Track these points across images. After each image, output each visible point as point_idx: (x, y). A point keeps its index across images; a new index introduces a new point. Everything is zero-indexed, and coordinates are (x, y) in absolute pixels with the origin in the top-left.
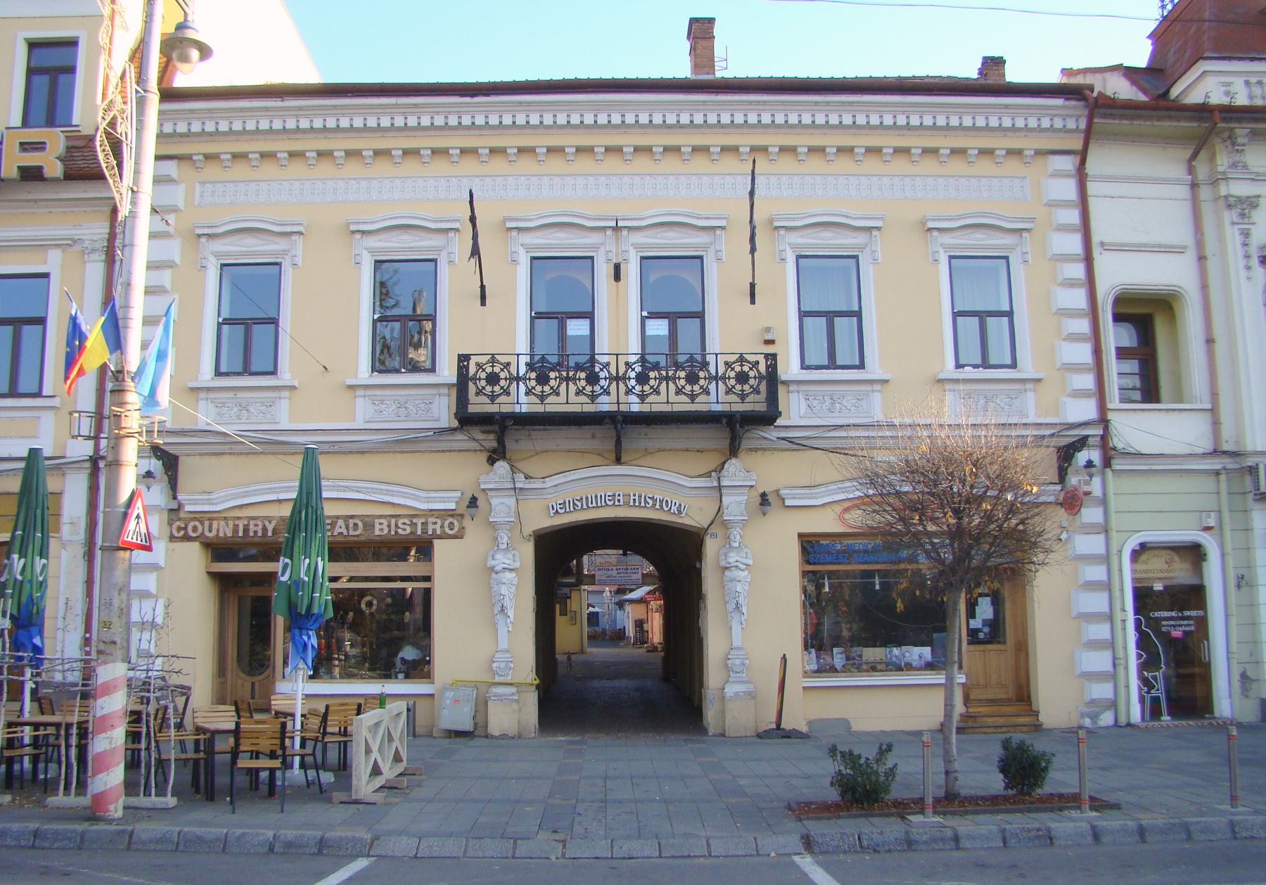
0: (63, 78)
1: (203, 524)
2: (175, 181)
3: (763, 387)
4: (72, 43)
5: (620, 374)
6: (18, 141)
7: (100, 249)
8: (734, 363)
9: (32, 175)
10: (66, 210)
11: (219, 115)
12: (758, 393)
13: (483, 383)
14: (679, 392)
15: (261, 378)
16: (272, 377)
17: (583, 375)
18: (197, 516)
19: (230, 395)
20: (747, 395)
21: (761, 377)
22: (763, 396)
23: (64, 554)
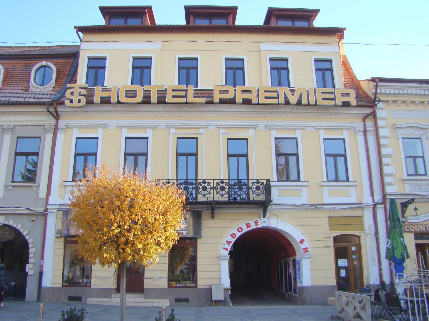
0: (100, 71)
1: (414, 226)
2: (383, 109)
4: (104, 59)
5: (215, 186)
6: (340, 93)
9: (346, 105)
11: (400, 88)
14: (217, 193)
15: (422, 176)
16: (426, 176)
17: (237, 187)
18: (412, 224)
19: (415, 182)
20: (260, 194)
23: (367, 238)
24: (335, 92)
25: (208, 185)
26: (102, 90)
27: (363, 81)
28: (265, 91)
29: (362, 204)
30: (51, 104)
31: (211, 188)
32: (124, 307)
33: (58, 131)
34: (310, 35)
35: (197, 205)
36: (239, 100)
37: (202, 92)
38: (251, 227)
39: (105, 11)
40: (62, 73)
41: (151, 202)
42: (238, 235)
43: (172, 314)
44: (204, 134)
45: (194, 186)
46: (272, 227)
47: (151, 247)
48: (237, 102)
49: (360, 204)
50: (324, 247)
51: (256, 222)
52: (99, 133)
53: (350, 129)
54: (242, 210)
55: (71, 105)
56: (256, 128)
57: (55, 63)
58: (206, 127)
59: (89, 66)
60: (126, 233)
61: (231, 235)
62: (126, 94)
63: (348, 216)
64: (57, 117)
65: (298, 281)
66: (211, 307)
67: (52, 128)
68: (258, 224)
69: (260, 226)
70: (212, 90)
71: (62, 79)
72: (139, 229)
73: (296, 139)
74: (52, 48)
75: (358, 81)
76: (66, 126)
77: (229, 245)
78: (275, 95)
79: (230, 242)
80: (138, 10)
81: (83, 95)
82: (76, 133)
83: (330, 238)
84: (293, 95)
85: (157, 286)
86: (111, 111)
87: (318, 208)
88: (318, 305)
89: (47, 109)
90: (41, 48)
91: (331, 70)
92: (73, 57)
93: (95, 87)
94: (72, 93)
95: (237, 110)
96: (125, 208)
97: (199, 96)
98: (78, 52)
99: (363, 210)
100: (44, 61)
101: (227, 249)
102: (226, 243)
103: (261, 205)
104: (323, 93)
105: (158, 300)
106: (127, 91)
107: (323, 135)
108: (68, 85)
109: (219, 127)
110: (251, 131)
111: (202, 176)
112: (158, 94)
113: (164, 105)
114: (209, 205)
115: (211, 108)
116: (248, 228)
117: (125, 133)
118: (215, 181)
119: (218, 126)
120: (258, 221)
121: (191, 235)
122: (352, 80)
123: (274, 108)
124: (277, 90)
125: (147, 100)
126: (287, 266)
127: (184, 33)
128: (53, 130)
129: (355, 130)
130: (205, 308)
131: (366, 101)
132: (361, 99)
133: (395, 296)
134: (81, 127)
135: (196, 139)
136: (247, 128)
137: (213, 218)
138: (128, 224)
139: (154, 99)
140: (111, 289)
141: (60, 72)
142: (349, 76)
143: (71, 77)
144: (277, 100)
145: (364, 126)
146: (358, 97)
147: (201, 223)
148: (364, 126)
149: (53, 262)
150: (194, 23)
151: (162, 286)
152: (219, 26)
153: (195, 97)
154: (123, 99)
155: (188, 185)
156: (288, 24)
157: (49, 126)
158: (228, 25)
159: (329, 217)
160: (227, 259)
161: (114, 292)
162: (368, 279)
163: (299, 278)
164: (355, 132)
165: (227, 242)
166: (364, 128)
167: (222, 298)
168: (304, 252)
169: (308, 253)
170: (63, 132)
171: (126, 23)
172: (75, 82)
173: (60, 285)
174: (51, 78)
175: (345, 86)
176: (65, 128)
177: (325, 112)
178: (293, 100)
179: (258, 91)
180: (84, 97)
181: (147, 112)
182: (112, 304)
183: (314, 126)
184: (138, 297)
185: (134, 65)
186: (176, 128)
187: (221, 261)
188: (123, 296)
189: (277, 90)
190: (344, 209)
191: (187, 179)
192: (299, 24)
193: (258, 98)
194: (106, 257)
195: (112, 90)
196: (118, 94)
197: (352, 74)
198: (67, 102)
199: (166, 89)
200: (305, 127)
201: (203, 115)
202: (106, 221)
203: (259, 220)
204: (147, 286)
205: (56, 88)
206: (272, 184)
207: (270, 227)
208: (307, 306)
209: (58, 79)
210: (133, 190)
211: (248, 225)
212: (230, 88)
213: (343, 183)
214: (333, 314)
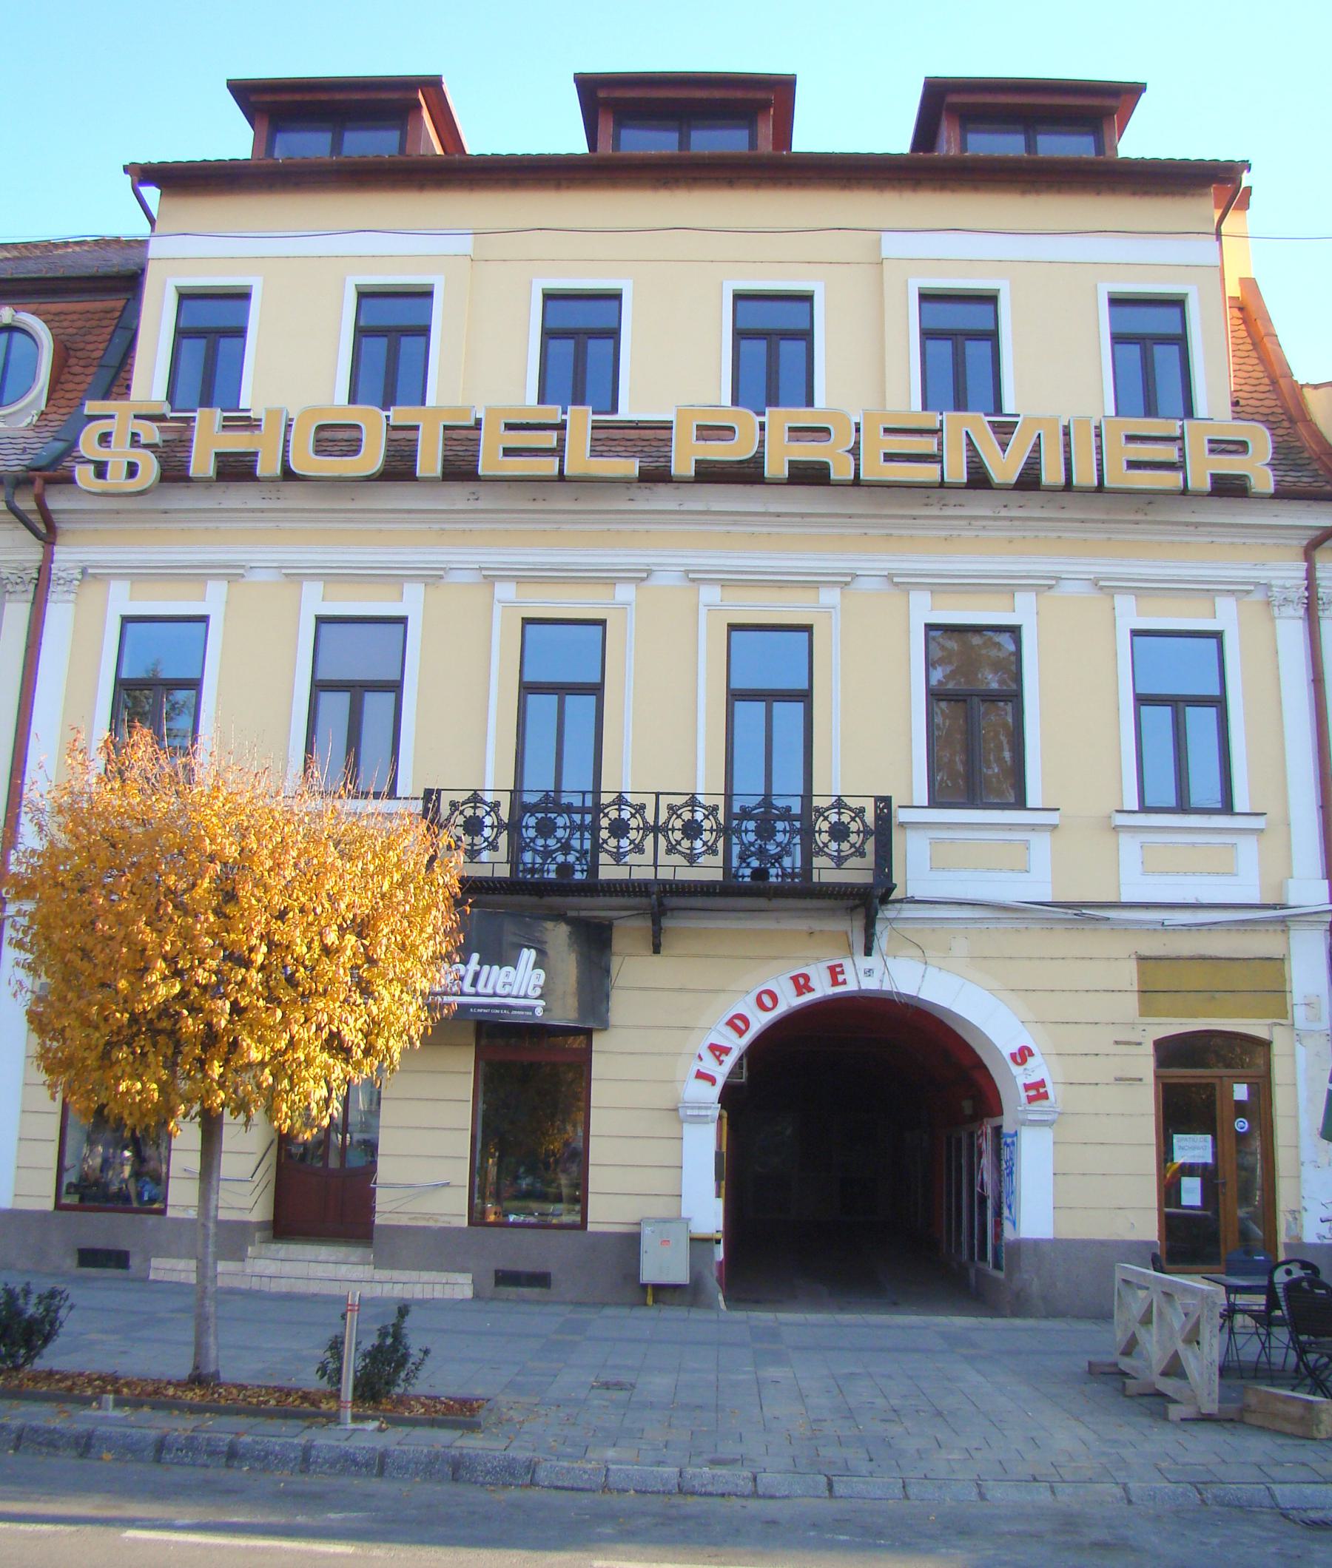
3: (870, 846)
4: (243, 296)
5: (661, 821)
7: (1296, 601)
8: (828, 809)
10: (1236, 540)
12: (862, 855)
13: (678, 835)
14: (671, 849)
17: (751, 825)
21: (866, 832)
22: (870, 859)
23: (1300, 1050)
24: (1183, 433)
25: (853, 819)
26: (224, 426)
27: (1316, 387)
28: (887, 431)
29: (1283, 907)
30: (22, 482)
31: (574, 828)
32: (211, 1289)
33: (52, 589)
34: (1098, 194)
35: (592, 896)
36: (776, 467)
37: (633, 431)
38: (811, 990)
39: (253, 98)
40: (79, 354)
41: (311, 881)
42: (760, 1021)
43: (397, 1326)
44: (634, 604)
45: (797, 824)
46: (898, 994)
47: (309, 1062)
48: (766, 474)
49: (1274, 907)
50: (1112, 1080)
51: (835, 972)
52: (212, 600)
53: (1248, 592)
54: (777, 920)
55: (98, 485)
56: (847, 584)
57: (55, 314)
58: (642, 579)
59: (550, 325)
60: (206, 1001)
61: (730, 1023)
62: (317, 441)
63: (1223, 956)
64: (47, 532)
65: (1007, 1218)
66: (640, 1312)
67: (27, 578)
68: (840, 978)
69: (851, 987)
70: (667, 426)
71: (77, 379)
72: (257, 987)
73: (1217, 636)
74: (60, 252)
75: (1297, 389)
76: (84, 572)
77: (721, 1062)
78: (926, 445)
79: (726, 1051)
80: (384, 96)
81: (147, 446)
82: (122, 599)
83: (1139, 1044)
84: (1004, 446)
85: (424, 1219)
86: (262, 511)
87: (1098, 919)
88: (1078, 1317)
89: (8, 503)
90: (16, 253)
91: (1181, 341)
92: (126, 290)
93: (195, 411)
94: (105, 438)
95: (773, 509)
96: (199, 901)
97: (618, 449)
98: (143, 270)
99: (1286, 931)
100: (7, 308)
101: (712, 1080)
102: (708, 1057)
103: (857, 902)
104: (1130, 438)
105: (426, 1276)
106: (321, 428)
107: (1130, 614)
108: (88, 404)
109: (695, 578)
110: (830, 596)
111: (828, 784)
112: (593, 439)
113: (472, 486)
114: (641, 896)
115: (662, 499)
116: (800, 993)
117: (316, 600)
118: (664, 801)
119: (691, 576)
120: (841, 965)
121: (566, 1014)
122: (1274, 382)
123: (926, 501)
124: (938, 426)
125: (401, 466)
126: (974, 1153)
127: (568, 188)
128: (32, 587)
129: (1270, 601)
130: (609, 1311)
131: (1321, 472)
132: (1297, 467)
133: (1323, 1292)
134: (140, 576)
135: (601, 627)
136: (812, 583)
137: (657, 949)
138: (212, 963)
139: (429, 461)
140: (243, 1226)
141: (71, 352)
142: (1260, 368)
143: (113, 371)
144: (938, 466)
145: (1306, 579)
146: (1285, 456)
147: (608, 971)
148: (1306, 579)
149: (24, 1111)
150: (616, 146)
151: (446, 1218)
152: (711, 157)
153: (595, 453)
154: (306, 461)
155: (553, 816)
156: (1008, 145)
157: (16, 568)
158: (685, 153)
159: (1142, 959)
160: (709, 1119)
161: (257, 1235)
162: (1295, 1219)
163: (1010, 1207)
164: (1269, 603)
165: (713, 1048)
166: (1307, 589)
167: (680, 1275)
168: (1031, 1099)
169: (1044, 1102)
170: (72, 597)
171: (684, 143)
172: (125, 391)
173: (49, 1205)
174: (34, 377)
175: (1238, 409)
176: (80, 577)
177: (1139, 517)
178: (1004, 467)
179: (858, 430)
180: (153, 456)
181: (406, 516)
182: (243, 1284)
183: (1092, 577)
184: (353, 1259)
185: (362, 323)
186: (519, 580)
187: (686, 1126)
188: (207, 1247)
189: (938, 426)
190: (1206, 927)
191: (768, 795)
192: (1056, 146)
193: (857, 459)
194: (128, 1090)
195: (263, 423)
196: (286, 441)
197: (1273, 358)
198: (84, 475)
199: (478, 423)
200: (1053, 582)
201: (378, 526)
202: (125, 950)
203: (847, 964)
204: (387, 1215)
205: (49, 417)
206: (901, 816)
207: (891, 992)
208: (1030, 1322)
209: (62, 380)
210: (243, 832)
211: (802, 981)
212: (745, 421)
213: (1207, 816)
214: (1092, 1358)
